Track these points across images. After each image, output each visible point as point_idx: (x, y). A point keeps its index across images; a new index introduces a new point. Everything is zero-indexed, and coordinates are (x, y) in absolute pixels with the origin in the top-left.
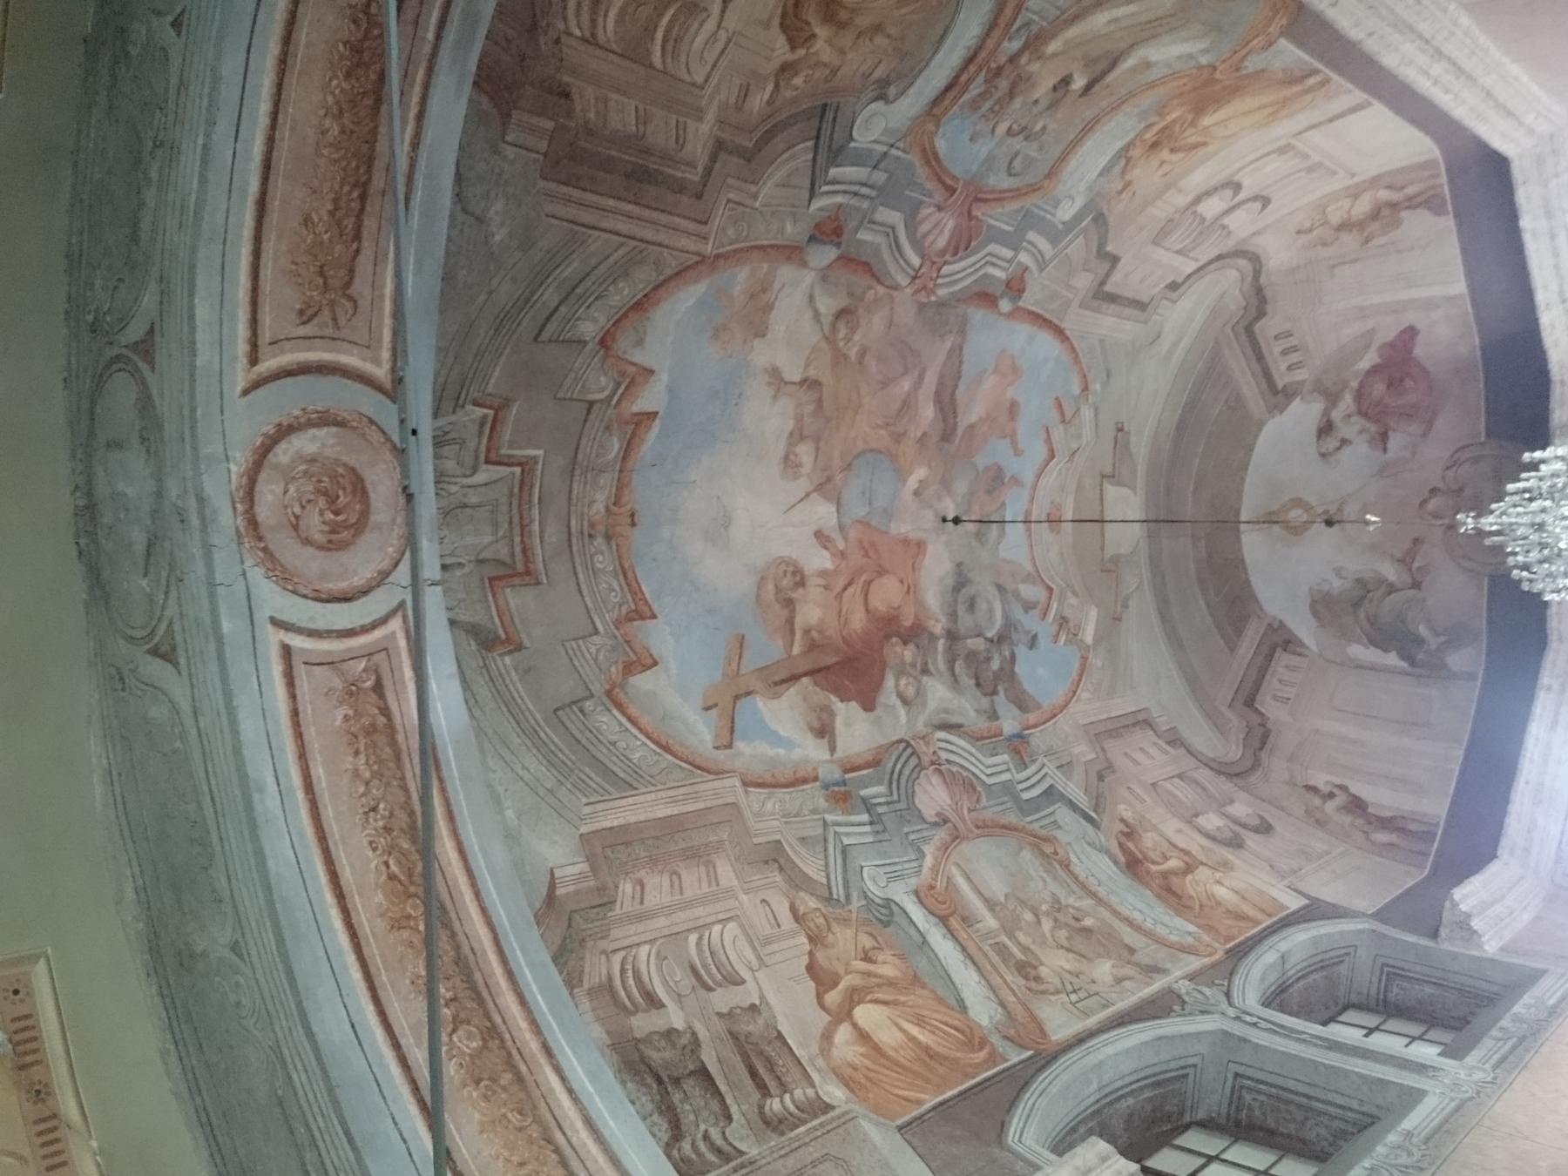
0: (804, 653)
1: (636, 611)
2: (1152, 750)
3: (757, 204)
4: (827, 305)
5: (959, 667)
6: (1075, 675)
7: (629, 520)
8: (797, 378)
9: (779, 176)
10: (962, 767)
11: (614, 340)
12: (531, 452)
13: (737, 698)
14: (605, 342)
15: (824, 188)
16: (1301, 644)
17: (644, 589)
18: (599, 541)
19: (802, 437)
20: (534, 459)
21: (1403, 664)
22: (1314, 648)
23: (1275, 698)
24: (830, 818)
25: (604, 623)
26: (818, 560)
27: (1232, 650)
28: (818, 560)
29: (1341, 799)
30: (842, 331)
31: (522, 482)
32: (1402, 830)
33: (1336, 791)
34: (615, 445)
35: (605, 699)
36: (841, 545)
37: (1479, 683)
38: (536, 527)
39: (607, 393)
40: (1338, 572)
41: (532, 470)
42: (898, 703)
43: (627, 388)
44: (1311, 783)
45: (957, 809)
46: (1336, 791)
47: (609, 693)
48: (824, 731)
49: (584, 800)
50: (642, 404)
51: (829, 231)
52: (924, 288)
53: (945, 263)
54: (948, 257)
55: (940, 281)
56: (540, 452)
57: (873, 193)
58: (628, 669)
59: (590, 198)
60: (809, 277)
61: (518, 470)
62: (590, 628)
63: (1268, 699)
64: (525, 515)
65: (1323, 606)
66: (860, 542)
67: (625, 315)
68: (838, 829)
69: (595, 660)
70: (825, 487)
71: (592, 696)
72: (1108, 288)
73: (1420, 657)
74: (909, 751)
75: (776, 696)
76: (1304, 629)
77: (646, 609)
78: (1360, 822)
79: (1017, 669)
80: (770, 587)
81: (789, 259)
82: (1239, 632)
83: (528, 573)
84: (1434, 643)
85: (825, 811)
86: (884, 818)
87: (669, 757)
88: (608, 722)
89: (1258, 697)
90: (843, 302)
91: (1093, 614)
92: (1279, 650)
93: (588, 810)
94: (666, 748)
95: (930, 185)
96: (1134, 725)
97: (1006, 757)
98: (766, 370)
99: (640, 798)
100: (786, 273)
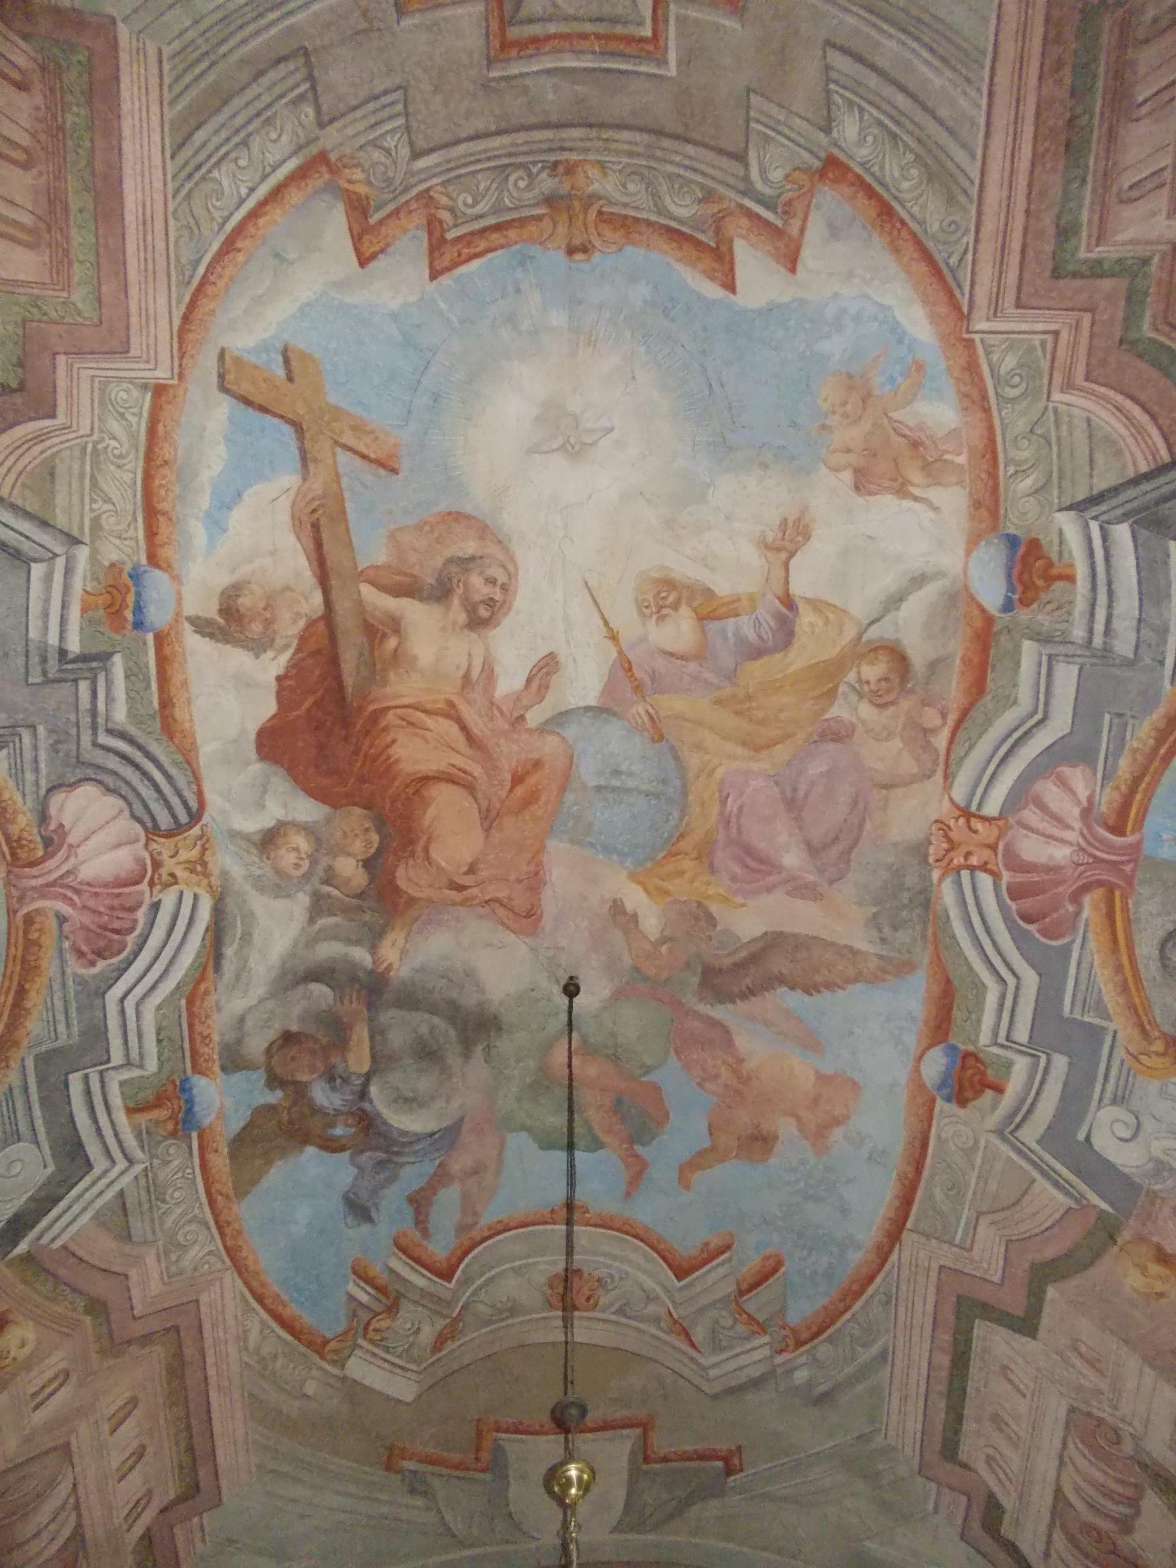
0: (359, 603)
1: (443, 240)
2: (134, 1484)
3: (1057, 396)
4: (910, 626)
5: (321, 993)
6: (292, 1310)
7: (577, 242)
8: (798, 588)
9: (1109, 422)
10: (145, 938)
11: (835, 181)
12: (672, 57)
13: (298, 428)
14: (833, 168)
15: (1094, 526)
17: (475, 264)
18: (547, 183)
19: (703, 618)
20: (663, 62)
24: (82, 554)
25: (430, 173)
26: (511, 655)
28: (511, 655)
30: (872, 671)
31: (629, 40)
34: (682, 208)
35: (314, 150)
36: (534, 717)
38: (570, 62)
39: (759, 185)
41: (649, 57)
42: (268, 822)
43: (767, 223)
45: (62, 886)
47: (322, 158)
48: (231, 621)
49: (167, 51)
50: (750, 259)
51: (1032, 569)
52: (952, 846)
53: (996, 876)
54: (1006, 877)
55: (965, 874)
56: (672, 70)
57: (1098, 641)
58: (358, 207)
59: (1028, 131)
60: (951, 560)
61: (647, 32)
62: (421, 144)
64: (584, 45)
66: (537, 764)
67: (871, 193)
68: (60, 563)
69: (375, 144)
70: (628, 677)
71: (322, 125)
72: (981, 1329)
74: (183, 818)
75: (297, 522)
77: (446, 261)
79: (311, 1150)
80: (470, 547)
81: (977, 504)
83: (505, 45)
85: (95, 552)
86: (67, 688)
87: (215, 247)
88: (277, 150)
90: (919, 655)
91: (404, 1389)
93: (152, 51)
94: (229, 246)
95: (1124, 764)
96: (190, 1449)
97: (152, 1065)
98: (805, 510)
99: (157, 160)
100: (953, 500)
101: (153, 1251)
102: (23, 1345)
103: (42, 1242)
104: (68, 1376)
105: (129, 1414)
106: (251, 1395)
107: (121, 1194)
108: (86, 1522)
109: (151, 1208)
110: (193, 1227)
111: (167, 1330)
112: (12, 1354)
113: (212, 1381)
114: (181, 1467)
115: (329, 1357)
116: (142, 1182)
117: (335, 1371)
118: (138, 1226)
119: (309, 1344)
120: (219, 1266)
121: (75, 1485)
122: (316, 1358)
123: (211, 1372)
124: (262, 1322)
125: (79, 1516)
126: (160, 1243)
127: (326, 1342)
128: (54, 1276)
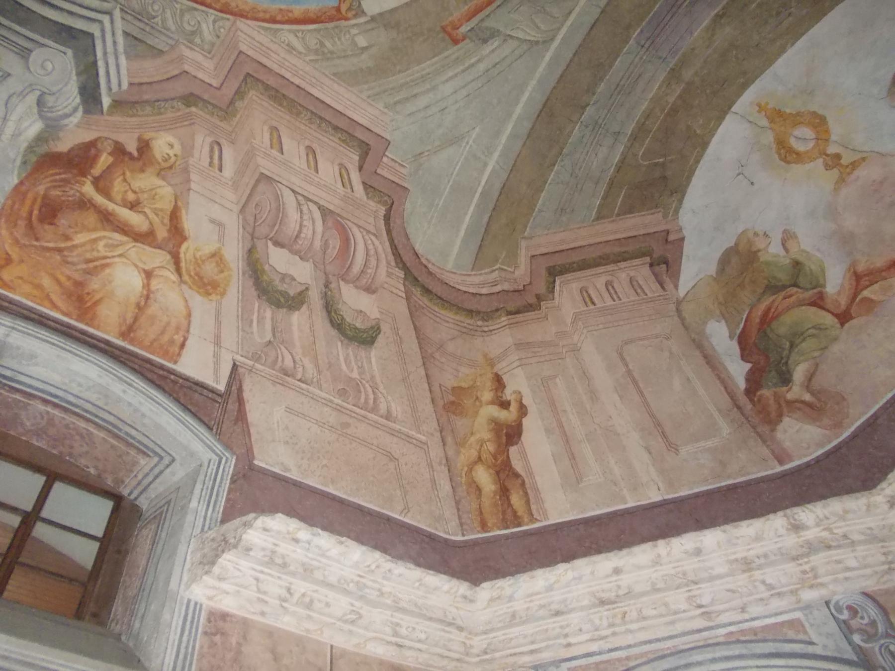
16: (675, 276)
21: (742, 384)
22: (682, 292)
23: (583, 290)
27: (599, 217)
29: (507, 416)
32: (504, 492)
33: (514, 407)
37: (779, 469)
40: (788, 237)
44: (505, 378)
46: (514, 407)
63: (575, 286)
65: (740, 261)
73: (765, 393)
76: (697, 266)
78: (491, 447)
82: (629, 209)
84: (796, 391)
89: (569, 276)
92: (648, 259)
96: (336, 128)
101: (183, 47)
102: (171, 146)
103: (114, 91)
104: (219, 144)
105: (280, 136)
106: (335, 74)
107: (126, 34)
108: (322, 203)
109: (152, 27)
110: (187, 17)
111: (245, 79)
112: (172, 155)
113: (303, 85)
114: (344, 141)
115: (350, 15)
116: (129, 18)
117: (362, 20)
118: (159, 42)
119: (331, 19)
120: (228, 24)
121: (293, 191)
122: (343, 23)
123: (297, 81)
124: (290, 31)
125: (315, 203)
126: (181, 40)
127: (338, 9)
128: (147, 102)
